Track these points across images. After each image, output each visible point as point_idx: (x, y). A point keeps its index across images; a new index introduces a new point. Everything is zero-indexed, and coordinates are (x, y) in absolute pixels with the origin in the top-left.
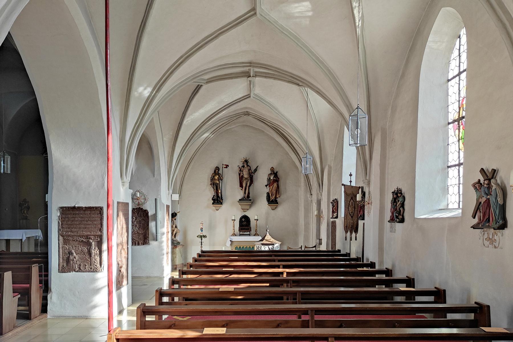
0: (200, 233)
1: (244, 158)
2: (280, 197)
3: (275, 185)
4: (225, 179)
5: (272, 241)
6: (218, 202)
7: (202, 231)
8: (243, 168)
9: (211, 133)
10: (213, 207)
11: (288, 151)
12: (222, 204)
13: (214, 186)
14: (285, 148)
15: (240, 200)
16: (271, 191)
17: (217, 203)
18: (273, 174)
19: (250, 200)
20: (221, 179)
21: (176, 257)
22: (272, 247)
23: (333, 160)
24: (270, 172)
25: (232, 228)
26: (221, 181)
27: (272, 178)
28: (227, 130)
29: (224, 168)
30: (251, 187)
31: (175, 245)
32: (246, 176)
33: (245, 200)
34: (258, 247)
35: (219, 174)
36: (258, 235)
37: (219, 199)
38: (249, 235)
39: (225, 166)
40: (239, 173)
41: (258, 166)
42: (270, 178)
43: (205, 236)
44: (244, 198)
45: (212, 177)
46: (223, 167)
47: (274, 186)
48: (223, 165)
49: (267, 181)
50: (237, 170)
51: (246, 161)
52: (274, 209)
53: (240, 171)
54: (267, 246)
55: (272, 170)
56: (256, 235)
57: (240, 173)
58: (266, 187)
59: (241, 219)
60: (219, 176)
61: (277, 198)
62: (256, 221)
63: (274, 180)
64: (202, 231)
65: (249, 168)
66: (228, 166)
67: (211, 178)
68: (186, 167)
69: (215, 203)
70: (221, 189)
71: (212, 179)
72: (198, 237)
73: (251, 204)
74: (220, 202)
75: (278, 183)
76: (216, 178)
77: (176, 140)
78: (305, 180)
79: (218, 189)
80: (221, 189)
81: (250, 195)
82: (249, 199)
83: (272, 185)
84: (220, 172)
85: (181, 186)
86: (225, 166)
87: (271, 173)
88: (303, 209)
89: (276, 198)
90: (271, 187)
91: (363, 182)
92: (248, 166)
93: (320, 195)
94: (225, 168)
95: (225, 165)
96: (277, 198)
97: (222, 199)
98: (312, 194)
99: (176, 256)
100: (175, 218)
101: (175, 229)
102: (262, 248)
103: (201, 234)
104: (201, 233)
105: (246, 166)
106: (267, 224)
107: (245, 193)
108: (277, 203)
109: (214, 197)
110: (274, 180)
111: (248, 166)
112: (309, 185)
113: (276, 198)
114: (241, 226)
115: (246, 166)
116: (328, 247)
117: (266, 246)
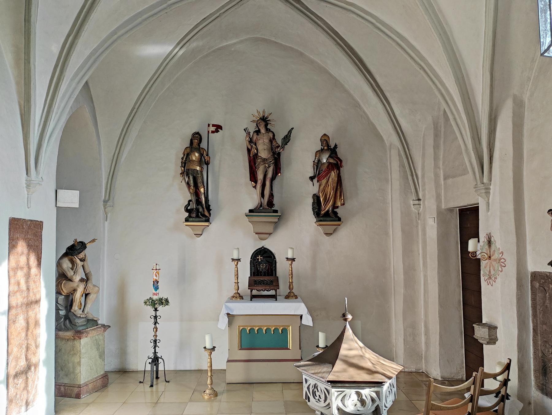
0: (150, 293)
1: (264, 112)
2: (344, 204)
3: (333, 174)
4: (216, 162)
5: (368, 365)
6: (197, 216)
7: (156, 288)
8: (258, 135)
9: (178, 44)
10: (187, 229)
11: (359, 100)
12: (208, 220)
13: (189, 178)
14: (352, 92)
15: (251, 211)
16: (324, 190)
17: (197, 219)
18: (326, 150)
19: (276, 211)
20: (204, 161)
21: (79, 363)
22: (374, 395)
23: (529, 78)
24: (319, 147)
25: (233, 280)
26: (205, 167)
27: (325, 161)
28: (219, 49)
29: (210, 134)
30: (276, 182)
31: (80, 329)
32: (264, 154)
33: (263, 211)
34: (315, 386)
35: (199, 149)
36: (296, 297)
37: (201, 210)
38: (274, 297)
39: (213, 129)
40: (248, 149)
41: (293, 128)
42: (319, 161)
43: (164, 302)
44: (261, 206)
45: (184, 155)
46: (208, 132)
47: (330, 179)
48: (209, 125)
49: (314, 167)
50: (242, 139)
51: (265, 120)
52: (331, 234)
53: (251, 141)
54: (353, 391)
55: (325, 140)
56: (290, 296)
57: (250, 147)
58: (312, 181)
59: (255, 256)
60: (201, 155)
61: (337, 207)
62: (290, 262)
63: (330, 164)
64: (156, 288)
65: (271, 135)
66: (222, 129)
67: (182, 159)
68: (123, 130)
69: (191, 219)
70: (205, 185)
71: (186, 161)
72: (145, 303)
73: (276, 220)
74: (204, 216)
75: (339, 173)
76: (194, 159)
77: (29, 5)
78: (402, 165)
79: (199, 185)
80: (205, 185)
81: (275, 201)
82: (273, 209)
83: (326, 176)
84: (204, 145)
85: (110, 177)
86: (213, 129)
87: (322, 150)
88: (399, 234)
89: (335, 207)
90: (324, 181)
91: (475, 189)
92: (268, 130)
93: (483, 191)
94: (213, 132)
95: (213, 126)
96: (337, 207)
97: (209, 210)
98: (421, 197)
99: (80, 361)
100: (81, 255)
101: (78, 286)
102: (334, 399)
103: (155, 298)
104: (154, 294)
105: (263, 131)
106: (314, 268)
107: (263, 195)
108: (339, 219)
109: (189, 204)
110: (330, 164)
111: (268, 130)
112: (412, 176)
113: (335, 207)
114: (254, 273)
115: (263, 131)
116: (523, 355)
117: (347, 391)
